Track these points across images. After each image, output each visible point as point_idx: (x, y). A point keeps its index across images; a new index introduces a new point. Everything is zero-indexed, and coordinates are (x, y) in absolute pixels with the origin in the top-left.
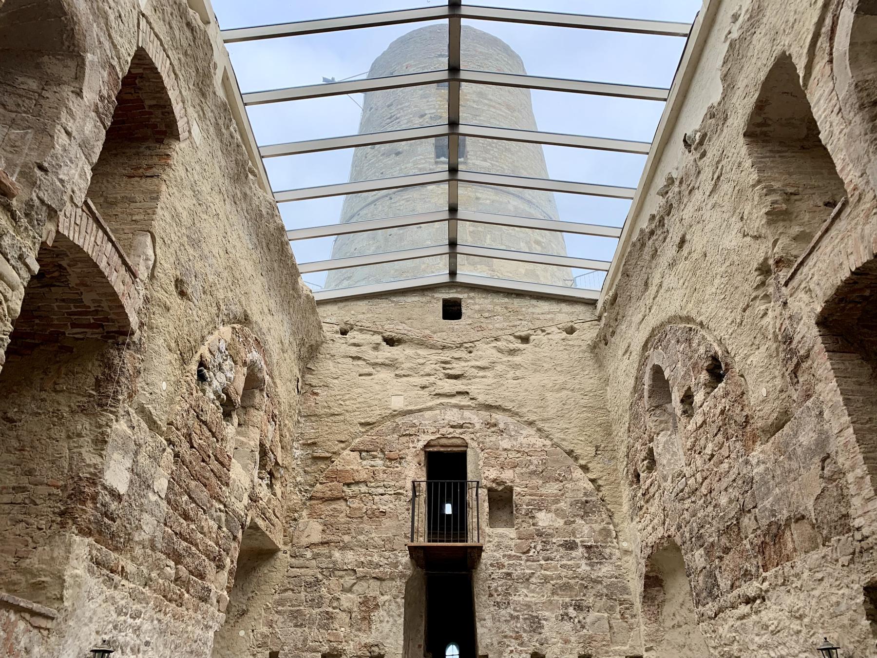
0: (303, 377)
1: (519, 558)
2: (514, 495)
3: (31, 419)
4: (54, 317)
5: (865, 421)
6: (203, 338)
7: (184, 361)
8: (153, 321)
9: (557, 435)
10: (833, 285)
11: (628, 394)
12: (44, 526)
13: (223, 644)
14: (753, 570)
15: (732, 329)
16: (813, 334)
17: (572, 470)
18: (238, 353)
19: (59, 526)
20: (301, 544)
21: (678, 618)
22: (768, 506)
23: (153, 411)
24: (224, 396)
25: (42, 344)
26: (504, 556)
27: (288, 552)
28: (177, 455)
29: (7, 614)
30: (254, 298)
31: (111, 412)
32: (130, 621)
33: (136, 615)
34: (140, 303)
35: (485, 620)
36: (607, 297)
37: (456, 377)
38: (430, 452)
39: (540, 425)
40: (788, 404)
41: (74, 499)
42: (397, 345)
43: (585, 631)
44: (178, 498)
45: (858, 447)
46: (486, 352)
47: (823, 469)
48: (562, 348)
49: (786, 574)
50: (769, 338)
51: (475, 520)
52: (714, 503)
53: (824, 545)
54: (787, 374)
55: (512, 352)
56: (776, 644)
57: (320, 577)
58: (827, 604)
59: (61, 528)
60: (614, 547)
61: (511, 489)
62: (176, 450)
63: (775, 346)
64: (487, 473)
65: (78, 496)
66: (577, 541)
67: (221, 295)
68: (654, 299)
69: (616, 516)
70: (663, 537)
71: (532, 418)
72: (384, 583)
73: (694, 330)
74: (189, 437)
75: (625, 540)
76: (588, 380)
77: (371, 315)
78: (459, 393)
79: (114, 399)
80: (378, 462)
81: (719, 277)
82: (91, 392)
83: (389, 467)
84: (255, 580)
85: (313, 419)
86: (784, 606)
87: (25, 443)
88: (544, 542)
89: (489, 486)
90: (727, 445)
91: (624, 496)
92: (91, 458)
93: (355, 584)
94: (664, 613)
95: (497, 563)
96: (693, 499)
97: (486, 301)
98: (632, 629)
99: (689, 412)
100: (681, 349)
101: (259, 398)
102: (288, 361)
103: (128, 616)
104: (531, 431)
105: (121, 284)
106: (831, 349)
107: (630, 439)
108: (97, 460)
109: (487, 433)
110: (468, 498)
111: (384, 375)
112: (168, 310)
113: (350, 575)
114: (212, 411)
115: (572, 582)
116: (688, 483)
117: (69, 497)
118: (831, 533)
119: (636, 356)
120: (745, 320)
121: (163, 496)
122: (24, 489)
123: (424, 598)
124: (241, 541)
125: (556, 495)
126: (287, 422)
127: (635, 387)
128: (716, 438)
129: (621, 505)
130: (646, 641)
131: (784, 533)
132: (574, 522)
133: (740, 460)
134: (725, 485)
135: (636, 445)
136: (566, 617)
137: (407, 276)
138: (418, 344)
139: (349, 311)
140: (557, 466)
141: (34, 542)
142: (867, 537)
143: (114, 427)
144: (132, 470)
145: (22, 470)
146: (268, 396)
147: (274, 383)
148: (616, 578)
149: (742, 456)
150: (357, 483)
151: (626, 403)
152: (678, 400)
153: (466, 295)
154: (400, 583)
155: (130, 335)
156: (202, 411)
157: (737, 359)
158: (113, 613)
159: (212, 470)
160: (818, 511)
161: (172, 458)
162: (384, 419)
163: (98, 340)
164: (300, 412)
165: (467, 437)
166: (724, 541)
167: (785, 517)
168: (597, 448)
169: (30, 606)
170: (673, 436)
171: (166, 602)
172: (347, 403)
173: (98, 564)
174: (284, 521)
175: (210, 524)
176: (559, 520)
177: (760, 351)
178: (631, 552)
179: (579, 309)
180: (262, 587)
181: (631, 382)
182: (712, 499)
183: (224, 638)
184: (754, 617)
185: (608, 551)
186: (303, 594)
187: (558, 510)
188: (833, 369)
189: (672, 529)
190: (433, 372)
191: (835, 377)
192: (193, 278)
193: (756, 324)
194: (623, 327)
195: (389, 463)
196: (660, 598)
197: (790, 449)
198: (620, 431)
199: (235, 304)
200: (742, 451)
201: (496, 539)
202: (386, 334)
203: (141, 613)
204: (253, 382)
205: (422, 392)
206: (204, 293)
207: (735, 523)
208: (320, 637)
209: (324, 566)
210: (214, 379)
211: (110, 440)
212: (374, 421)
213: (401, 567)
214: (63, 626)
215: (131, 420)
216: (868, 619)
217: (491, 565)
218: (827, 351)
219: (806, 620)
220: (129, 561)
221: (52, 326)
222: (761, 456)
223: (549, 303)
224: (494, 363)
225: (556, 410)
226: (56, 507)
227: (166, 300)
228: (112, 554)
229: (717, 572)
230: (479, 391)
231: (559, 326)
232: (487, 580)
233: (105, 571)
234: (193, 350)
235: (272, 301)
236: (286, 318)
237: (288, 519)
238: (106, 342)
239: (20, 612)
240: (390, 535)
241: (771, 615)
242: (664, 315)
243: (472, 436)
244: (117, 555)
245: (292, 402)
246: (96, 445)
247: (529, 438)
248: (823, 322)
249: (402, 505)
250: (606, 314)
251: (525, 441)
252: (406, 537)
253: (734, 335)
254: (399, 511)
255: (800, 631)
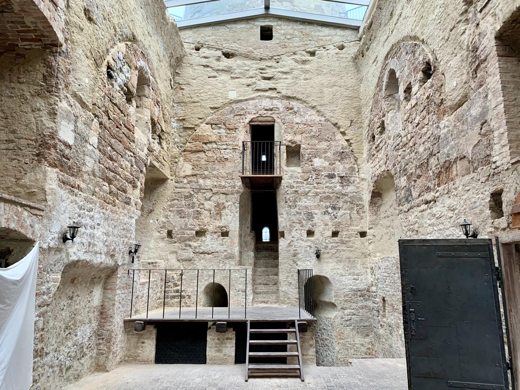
0: (174, 78)
1: (303, 183)
2: (301, 149)
3: (8, 100)
4: (9, 34)
5: (512, 100)
6: (108, 50)
7: (97, 66)
8: (73, 37)
9: (329, 114)
10: (510, 10)
11: (373, 88)
12: (28, 162)
13: (141, 226)
14: (432, 187)
15: (442, 43)
16: (492, 45)
17: (336, 135)
18: (131, 61)
19: (37, 162)
20: (181, 176)
21: (388, 213)
22: (446, 152)
23: (82, 96)
24: (125, 88)
25: (5, 52)
26: (294, 182)
27: (174, 180)
28: (101, 124)
29: (16, 208)
30: (138, 24)
31: (56, 96)
32: (87, 213)
33: (90, 210)
34: (63, 25)
35: (283, 214)
36: (366, 24)
37: (269, 79)
38: (253, 125)
39: (319, 108)
40: (468, 91)
41: (43, 147)
42: (232, 58)
43: (337, 219)
44: (105, 148)
45: (504, 116)
46: (288, 62)
47: (481, 129)
48: (335, 59)
49: (450, 188)
50: (464, 48)
51: (278, 163)
52: (415, 151)
53: (473, 172)
54: (470, 72)
55: (304, 62)
56: (438, 223)
57: (192, 193)
58: (469, 202)
59: (39, 163)
60: (356, 177)
61: (299, 146)
62: (100, 120)
63: (466, 54)
64: (286, 137)
65: (44, 145)
66: (336, 173)
67: (115, 21)
68: (395, 25)
69: (359, 160)
70: (384, 171)
71: (314, 104)
72: (228, 196)
73: (418, 45)
74: (106, 112)
75: (363, 173)
76: (350, 80)
77: (214, 37)
78: (271, 89)
79: (57, 88)
80: (223, 131)
81: (438, 7)
82: (41, 83)
83: (228, 134)
84: (156, 195)
85: (182, 104)
86: (446, 204)
87: (8, 114)
88: (317, 174)
89: (287, 144)
90: (428, 117)
91: (365, 149)
92: (49, 124)
93: (212, 196)
94: (381, 211)
95: (290, 186)
96: (404, 149)
97: (289, 27)
98: (362, 219)
99: (408, 98)
100: (408, 58)
101: (147, 91)
102: (163, 67)
103: (86, 210)
104: (313, 112)
105: (48, 10)
106: (501, 54)
107: (371, 116)
108: (53, 125)
109: (287, 114)
110: (275, 151)
111: (224, 77)
112: (82, 30)
113: (209, 192)
114: (120, 98)
115: (331, 195)
116: (403, 140)
117: (40, 146)
118: (478, 165)
119: (380, 64)
120: (451, 37)
121: (96, 147)
122: (12, 141)
123: (250, 204)
124: (145, 173)
125: (326, 149)
126: (166, 106)
127: (378, 84)
128: (422, 113)
129: (362, 154)
130: (369, 224)
131: (452, 166)
132: (334, 163)
133: (434, 126)
134: (423, 140)
135: (375, 119)
136: (326, 213)
137: (237, 10)
138: (245, 57)
139: (200, 34)
140: (327, 132)
141: (25, 171)
142: (498, 167)
143: (59, 105)
144: (75, 131)
145: (9, 130)
146: (153, 90)
147: (156, 81)
148: (356, 193)
149: (435, 123)
150: (211, 143)
151: (371, 94)
152: (403, 91)
153: (275, 24)
154: (237, 196)
155: (60, 46)
156: (113, 97)
157: (441, 63)
158: (77, 208)
159: (123, 133)
160: (474, 153)
161: (98, 125)
162: (225, 105)
163: (40, 49)
164: (174, 100)
165: (275, 116)
166: (418, 172)
167: (455, 157)
168: (352, 121)
169: (29, 204)
170: (397, 113)
171: (106, 204)
172: (202, 95)
173: (64, 183)
174: (170, 163)
175: (126, 164)
176: (326, 162)
177: (456, 57)
178: (366, 179)
179: (348, 32)
180: (161, 198)
181: (376, 80)
182: (415, 149)
183: (142, 224)
184: (429, 211)
185: (352, 179)
186: (183, 202)
187: (326, 157)
188: (499, 67)
189: (390, 166)
190: (254, 75)
191: (500, 72)
192: (96, 8)
193: (457, 39)
194: (374, 45)
195: (229, 132)
196: (380, 202)
197: (464, 118)
198: (366, 111)
199: (126, 28)
200: (436, 121)
201: (290, 173)
202: (224, 50)
203: (93, 209)
204: (143, 81)
205: (247, 89)
206: (105, 19)
207: (426, 161)
208: (194, 223)
209: (194, 187)
210: (118, 78)
211: (58, 113)
212: (219, 106)
213: (237, 188)
214: (50, 215)
215: (69, 101)
216: (490, 210)
217: (287, 187)
218: (498, 56)
219: (456, 211)
220: (81, 182)
221: (9, 40)
222: (447, 123)
223: (329, 28)
224: (292, 69)
225: (329, 99)
226: (34, 151)
227: (80, 23)
228: (71, 178)
229: (412, 188)
230: (283, 87)
231: (334, 44)
232: (284, 194)
233: (68, 187)
234: (102, 58)
235: (150, 26)
236: (160, 39)
237: (172, 162)
238: (45, 51)
239: (24, 206)
240: (230, 171)
241: (438, 210)
242: (400, 35)
243: (278, 115)
244: (74, 179)
245: (168, 93)
246: (50, 116)
247: (312, 116)
248: (500, 37)
249: (237, 156)
250: (364, 36)
251: (309, 118)
252: (239, 172)
253: (442, 48)
254: (235, 158)
255: (452, 217)
